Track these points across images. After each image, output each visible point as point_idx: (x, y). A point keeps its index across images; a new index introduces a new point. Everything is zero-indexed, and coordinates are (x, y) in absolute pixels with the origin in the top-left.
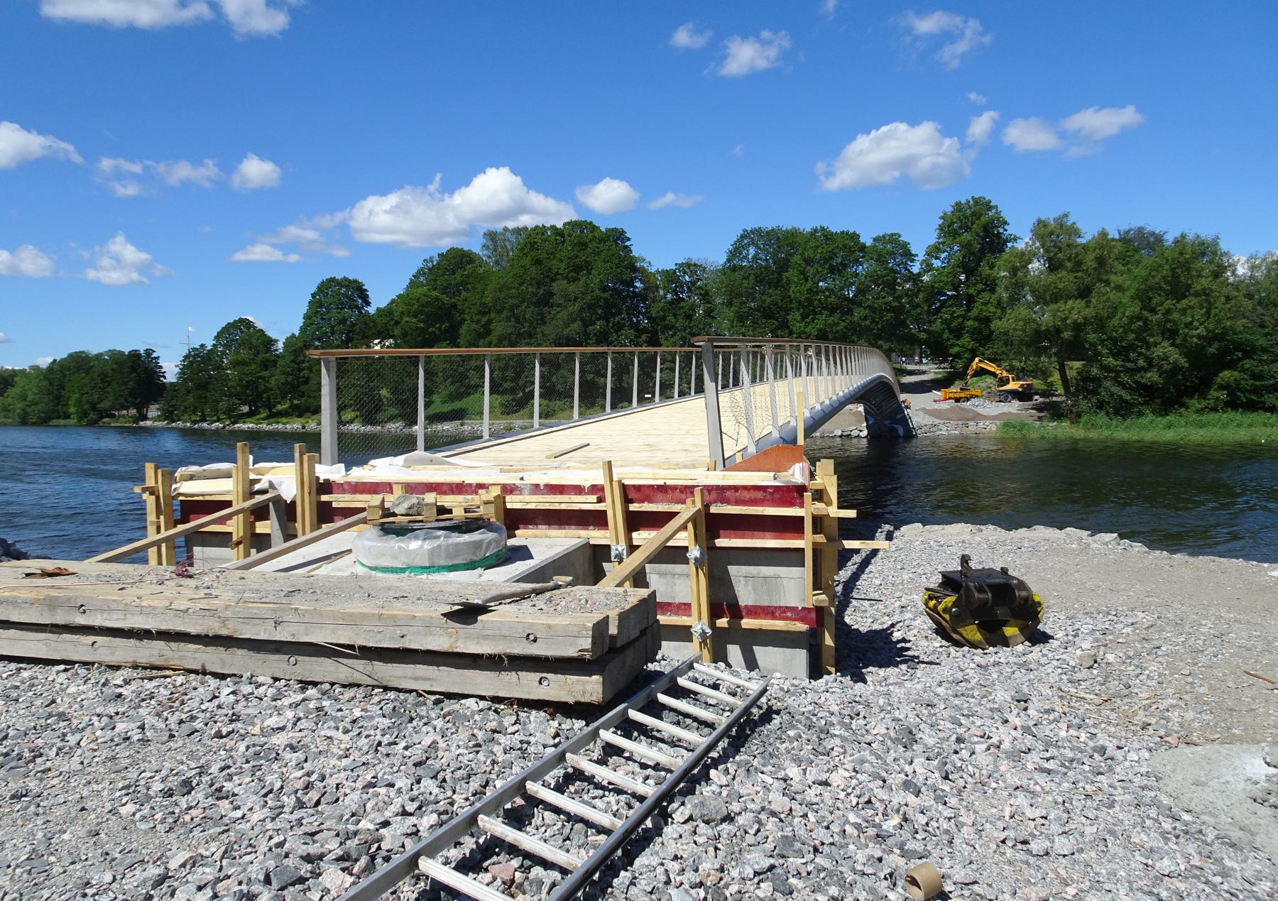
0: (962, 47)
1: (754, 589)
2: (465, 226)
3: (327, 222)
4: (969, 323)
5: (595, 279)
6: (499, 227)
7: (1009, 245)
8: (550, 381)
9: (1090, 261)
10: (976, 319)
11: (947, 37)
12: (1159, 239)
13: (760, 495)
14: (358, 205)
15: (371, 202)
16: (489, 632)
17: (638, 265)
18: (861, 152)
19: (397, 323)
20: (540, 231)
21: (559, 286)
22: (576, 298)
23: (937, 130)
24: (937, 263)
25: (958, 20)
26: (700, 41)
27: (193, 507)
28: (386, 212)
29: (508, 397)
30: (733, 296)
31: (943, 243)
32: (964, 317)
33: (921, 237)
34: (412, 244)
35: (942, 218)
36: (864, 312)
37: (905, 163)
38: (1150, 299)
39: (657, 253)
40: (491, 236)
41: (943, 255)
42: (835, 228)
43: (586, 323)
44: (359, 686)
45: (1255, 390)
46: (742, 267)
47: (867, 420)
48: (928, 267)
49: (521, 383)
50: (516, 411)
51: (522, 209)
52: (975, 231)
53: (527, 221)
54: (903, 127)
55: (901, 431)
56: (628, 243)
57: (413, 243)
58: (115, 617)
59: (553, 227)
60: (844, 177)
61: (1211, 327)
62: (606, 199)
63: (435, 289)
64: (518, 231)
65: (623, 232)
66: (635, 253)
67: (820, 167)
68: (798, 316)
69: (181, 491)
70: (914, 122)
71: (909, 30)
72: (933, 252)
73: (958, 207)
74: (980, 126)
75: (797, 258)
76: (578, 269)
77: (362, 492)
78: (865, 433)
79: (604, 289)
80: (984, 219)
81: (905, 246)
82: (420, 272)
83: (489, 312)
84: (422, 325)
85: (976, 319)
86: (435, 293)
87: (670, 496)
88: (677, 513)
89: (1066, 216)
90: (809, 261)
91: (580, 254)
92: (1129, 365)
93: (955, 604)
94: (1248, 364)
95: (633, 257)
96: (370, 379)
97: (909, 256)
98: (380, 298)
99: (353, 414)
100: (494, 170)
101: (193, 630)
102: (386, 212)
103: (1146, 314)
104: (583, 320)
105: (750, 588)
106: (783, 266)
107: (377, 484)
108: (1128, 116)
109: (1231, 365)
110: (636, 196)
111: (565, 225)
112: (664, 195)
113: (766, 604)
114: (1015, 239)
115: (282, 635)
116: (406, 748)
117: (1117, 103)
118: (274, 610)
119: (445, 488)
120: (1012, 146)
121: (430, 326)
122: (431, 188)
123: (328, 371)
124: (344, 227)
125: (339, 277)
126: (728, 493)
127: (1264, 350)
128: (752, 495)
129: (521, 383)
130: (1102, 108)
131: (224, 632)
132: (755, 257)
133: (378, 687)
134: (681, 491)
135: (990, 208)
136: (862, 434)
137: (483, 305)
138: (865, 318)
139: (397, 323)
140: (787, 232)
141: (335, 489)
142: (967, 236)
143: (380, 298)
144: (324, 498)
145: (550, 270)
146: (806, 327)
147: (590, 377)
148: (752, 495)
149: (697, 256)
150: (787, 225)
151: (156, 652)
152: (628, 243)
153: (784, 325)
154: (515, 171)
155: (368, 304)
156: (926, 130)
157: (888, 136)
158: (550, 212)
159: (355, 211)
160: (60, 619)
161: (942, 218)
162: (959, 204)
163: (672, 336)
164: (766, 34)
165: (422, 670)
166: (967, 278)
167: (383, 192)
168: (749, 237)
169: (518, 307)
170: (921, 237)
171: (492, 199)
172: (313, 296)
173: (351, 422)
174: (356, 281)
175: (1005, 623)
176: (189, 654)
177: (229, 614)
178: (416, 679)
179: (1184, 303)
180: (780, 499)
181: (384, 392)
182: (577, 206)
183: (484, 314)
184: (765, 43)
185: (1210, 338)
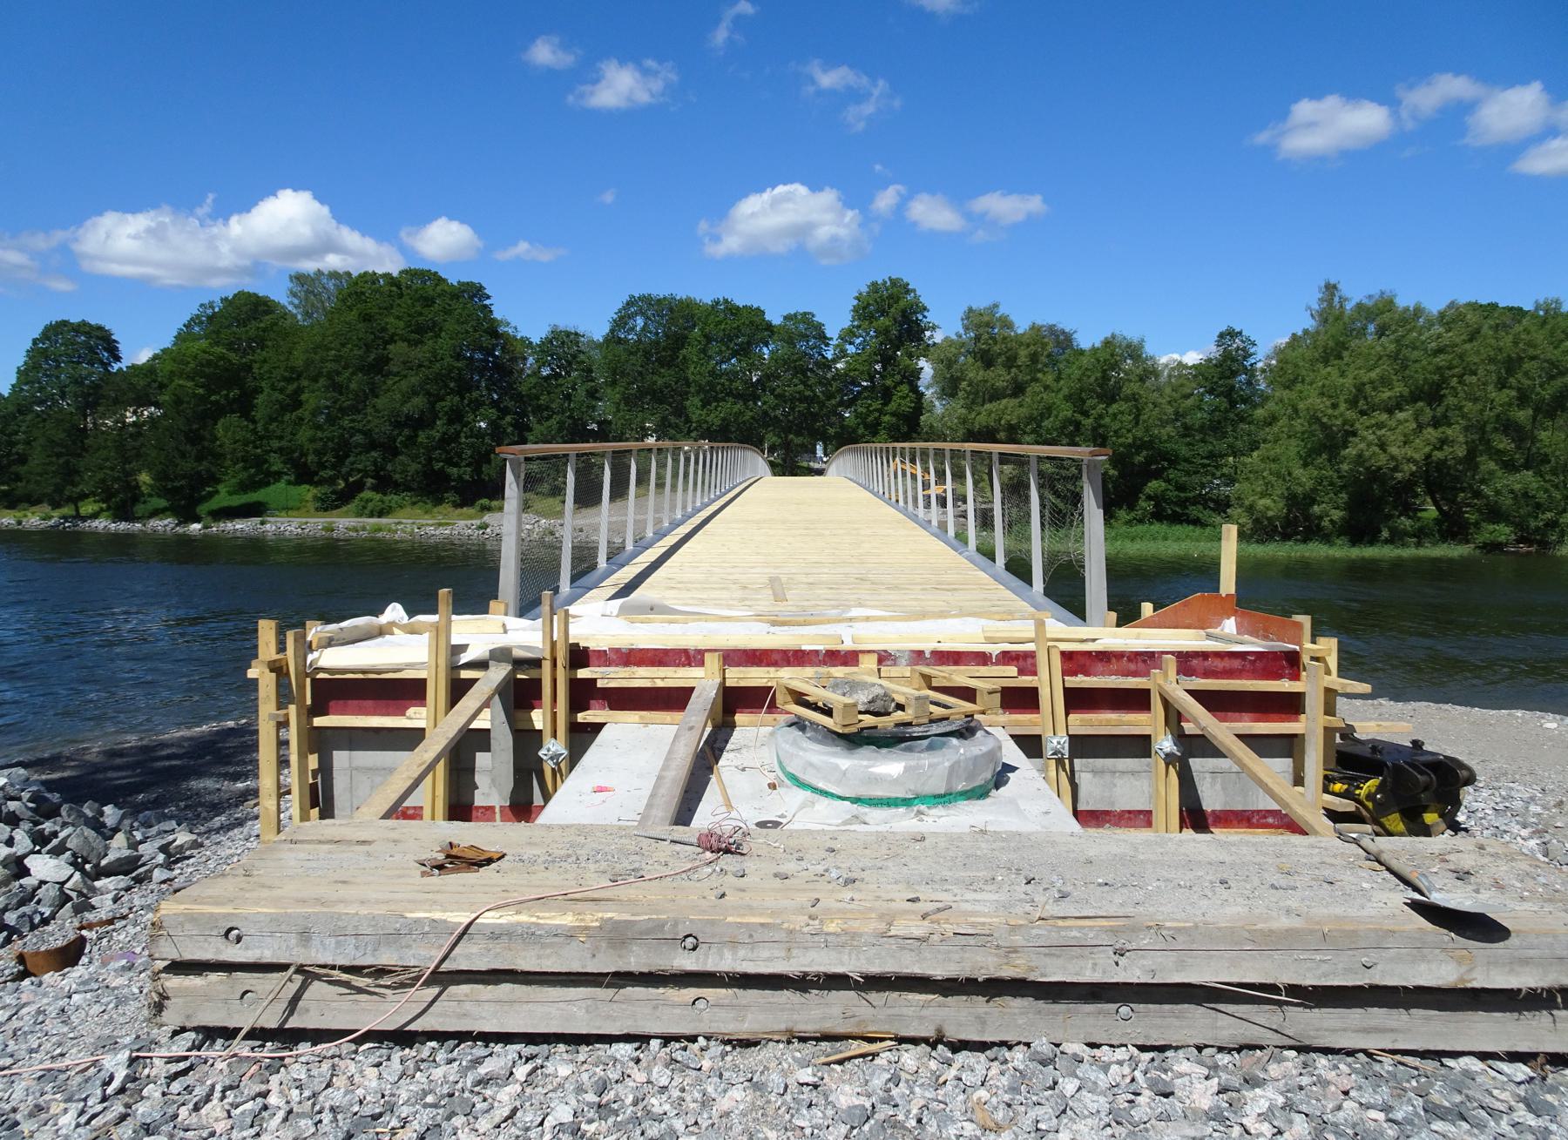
0: (869, 109)
1: (1224, 789)
2: (247, 262)
3: (40, 242)
4: (886, 418)
5: (445, 344)
6: (309, 266)
7: (928, 333)
8: (383, 469)
9: (1023, 355)
10: (893, 414)
11: (853, 96)
12: (1064, 340)
13: (1237, 664)
14: (89, 223)
15: (109, 220)
16: (1531, 953)
17: (502, 329)
18: (753, 215)
19: (162, 386)
20: (370, 278)
21: (397, 349)
22: (420, 366)
23: (839, 199)
24: (851, 349)
25: (865, 80)
26: (565, 60)
27: (337, 691)
28: (129, 236)
29: (326, 489)
30: (616, 373)
31: (859, 327)
32: (880, 411)
33: (836, 318)
34: (168, 281)
35: (857, 298)
37: (802, 231)
38: (1084, 402)
39: (527, 316)
40: (300, 278)
41: (858, 341)
42: (740, 302)
43: (435, 399)
44: (1261, 1048)
45: (1183, 503)
46: (626, 341)
48: (843, 353)
49: (344, 470)
50: (337, 507)
51: (329, 246)
52: (893, 317)
53: (333, 262)
54: (800, 190)
56: (487, 302)
57: (169, 279)
58: (765, 954)
59: (387, 276)
60: (731, 243)
61: (1139, 434)
62: (443, 243)
63: (217, 343)
64: (334, 275)
65: (481, 288)
66: (497, 315)
67: (703, 226)
68: (696, 401)
69: (322, 663)
70: (815, 187)
71: (813, 81)
72: (848, 335)
73: (874, 287)
74: (886, 200)
76: (420, 331)
77: (639, 664)
79: (458, 356)
80: (902, 304)
81: (819, 327)
82: (195, 320)
83: (298, 379)
84: (201, 391)
85: (893, 414)
86: (219, 350)
87: (1114, 666)
88: (1189, 692)
89: (996, 306)
90: (708, 338)
91: (425, 311)
92: (1064, 473)
93: (1380, 789)
94: (1172, 473)
95: (494, 320)
96: (127, 461)
97: (823, 338)
98: (137, 352)
99: (96, 507)
100: (289, 192)
101: (939, 972)
102: (129, 236)
103: (1078, 417)
104: (428, 393)
105: (1218, 786)
106: (679, 341)
107: (666, 652)
108: (1035, 204)
109: (1157, 475)
110: (480, 244)
111: (401, 272)
112: (515, 243)
113: (1240, 808)
114: (934, 328)
115: (1132, 972)
117: (1025, 190)
118: (1114, 931)
119: (775, 657)
120: (915, 224)
121: (211, 392)
122: (200, 212)
123: (517, 477)
124: (65, 250)
125: (75, 319)
126: (1195, 662)
127: (1186, 460)
128: (1220, 664)
129: (344, 470)
130: (1010, 192)
131: (1007, 973)
132: (643, 329)
133: (1291, 1048)
134: (1130, 660)
135: (908, 291)
137: (292, 370)
139: (162, 386)
140: (681, 301)
141: (593, 659)
142: (883, 321)
143: (139, 349)
144: (583, 673)
145: (384, 330)
147: (438, 466)
148: (1220, 664)
149: (569, 321)
150: (681, 294)
151: (836, 1011)
152: (487, 302)
153: (680, 411)
154: (320, 198)
155: (118, 359)
156: (828, 197)
157: (787, 198)
158: (366, 254)
159: (81, 231)
160: (635, 961)
161: (857, 298)
162: (874, 284)
163: (547, 419)
164: (650, 63)
165: (1377, 1016)
166: (884, 367)
167: (131, 206)
169: (338, 373)
170: (836, 318)
171: (284, 232)
172: (35, 341)
173: (95, 516)
174: (100, 328)
175: (1425, 809)
176: (909, 1011)
177: (1018, 940)
178: (1367, 1031)
179: (1115, 407)
180: (1264, 669)
181: (144, 478)
182: (404, 250)
183: (289, 380)
184: (646, 73)
185: (1139, 446)
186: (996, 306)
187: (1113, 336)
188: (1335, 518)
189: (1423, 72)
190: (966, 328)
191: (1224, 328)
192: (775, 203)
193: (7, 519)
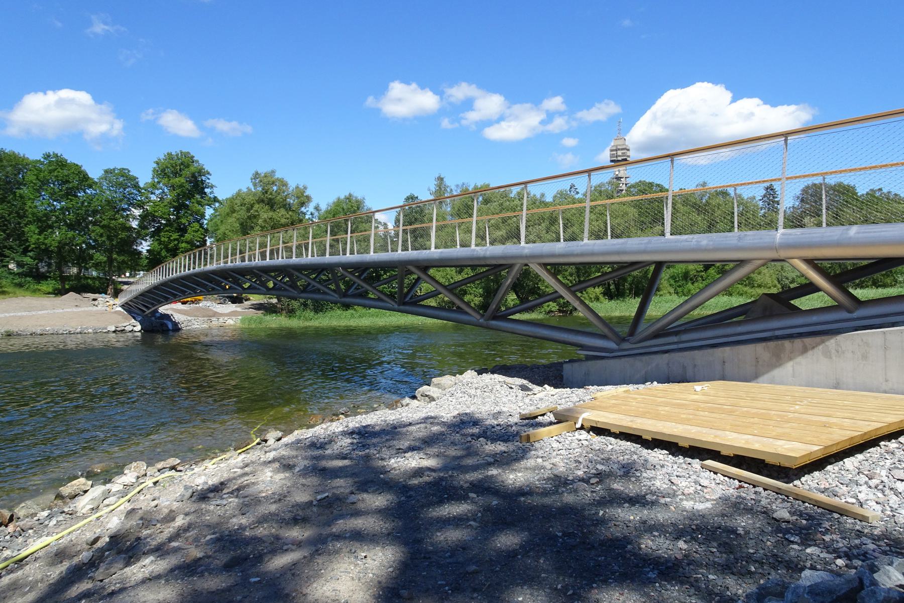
36: (99, 230)
41: (157, 192)
47: (134, 318)
55: (170, 326)
78: (139, 328)
80: (192, 169)
89: (273, 172)
136: (135, 329)
138: (101, 236)
146: (45, 239)
162: (170, 154)
186: (273, 172)
187: (350, 195)
188: (477, 303)
189: (454, 82)
190: (255, 185)
191: (408, 194)
192: (61, 103)
193: (2, 315)
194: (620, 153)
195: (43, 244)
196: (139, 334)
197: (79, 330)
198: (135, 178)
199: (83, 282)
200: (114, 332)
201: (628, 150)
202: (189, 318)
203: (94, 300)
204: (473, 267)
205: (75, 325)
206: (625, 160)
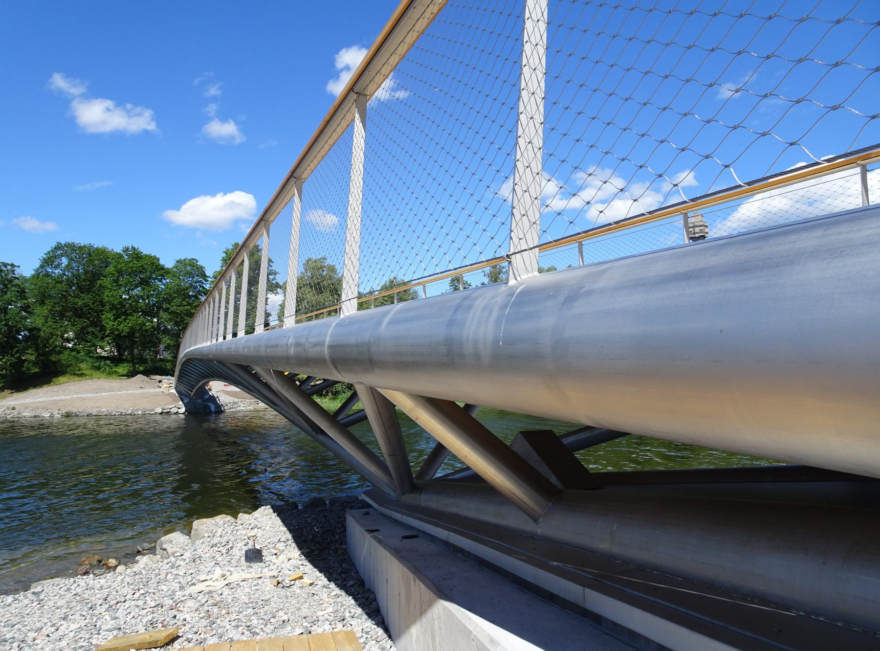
47: (182, 400)
55: (213, 408)
68: (110, 315)
75: (111, 269)
78: (183, 410)
89: (324, 259)
90: (120, 272)
97: (204, 276)
108: (141, 122)
116: (273, 480)
140: (97, 249)
146: (119, 325)
150: (98, 243)
164: (129, 106)
168: (61, 249)
194: (697, 230)
195: (117, 330)
196: (183, 416)
197: (130, 412)
198: (202, 267)
199: (158, 365)
200: (161, 413)
201: (706, 226)
202: (236, 400)
203: (160, 382)
204: (374, 485)
205: (127, 408)
206: (703, 237)
